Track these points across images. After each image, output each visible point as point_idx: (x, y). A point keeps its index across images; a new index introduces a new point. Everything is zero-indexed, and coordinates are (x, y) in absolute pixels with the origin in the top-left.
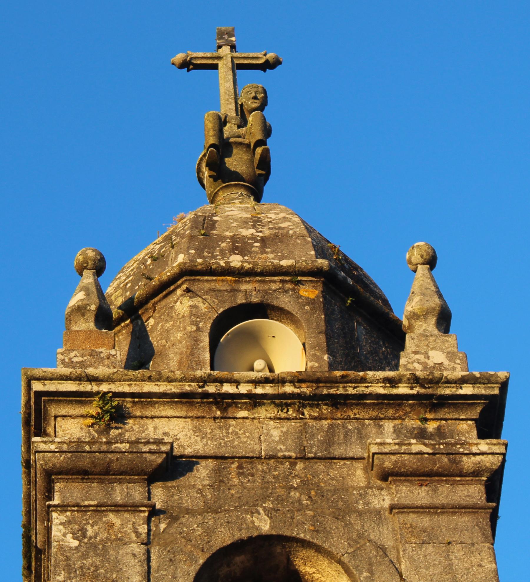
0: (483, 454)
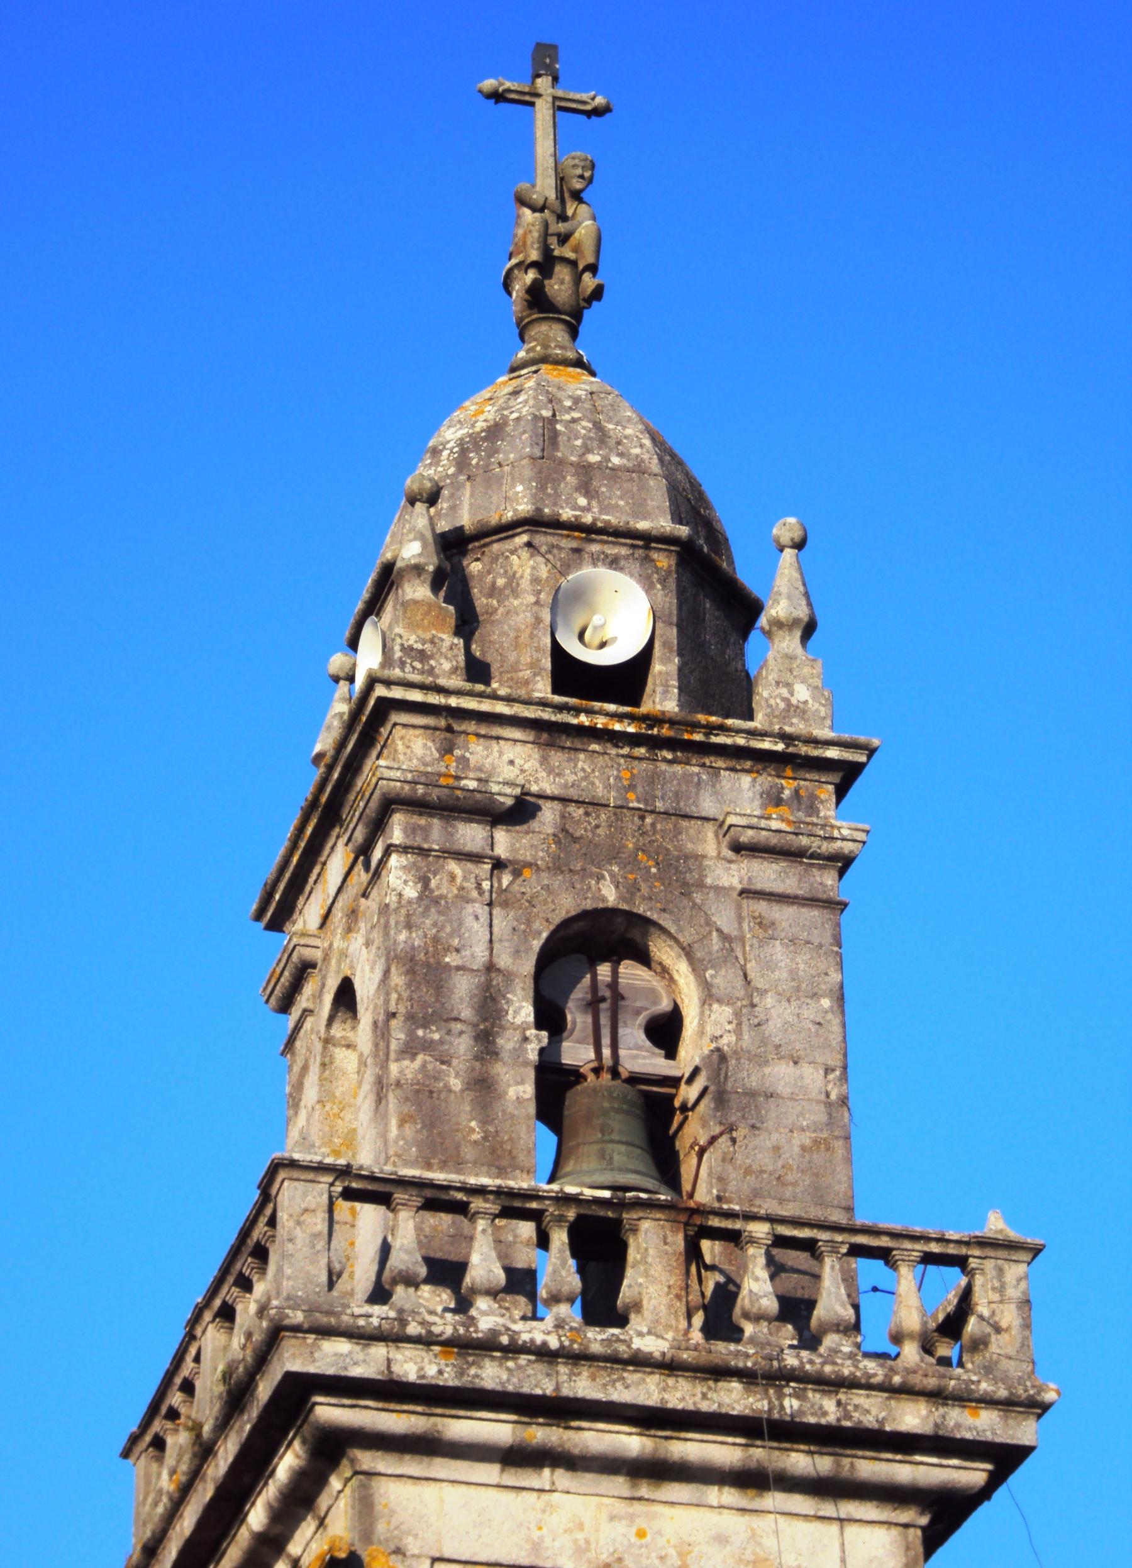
0: (844, 839)
